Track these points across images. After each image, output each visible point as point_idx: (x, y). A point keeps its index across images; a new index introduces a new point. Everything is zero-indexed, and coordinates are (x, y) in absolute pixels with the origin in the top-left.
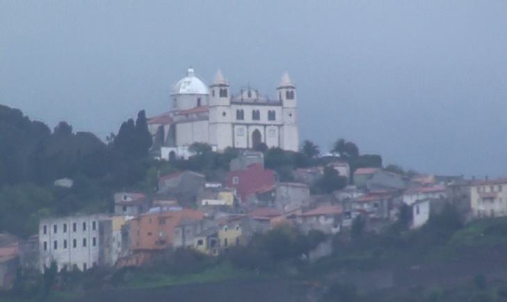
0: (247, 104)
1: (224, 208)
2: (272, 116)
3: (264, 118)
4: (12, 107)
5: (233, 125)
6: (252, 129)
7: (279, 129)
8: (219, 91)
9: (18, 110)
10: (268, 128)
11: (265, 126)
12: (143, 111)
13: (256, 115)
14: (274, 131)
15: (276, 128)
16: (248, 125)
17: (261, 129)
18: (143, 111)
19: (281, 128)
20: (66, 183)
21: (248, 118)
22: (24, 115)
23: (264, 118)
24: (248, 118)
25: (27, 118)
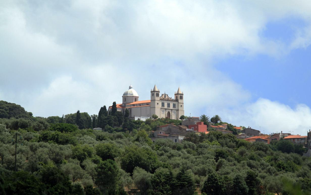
0: (165, 100)
1: (36, 137)
2: (174, 106)
3: (171, 107)
4: (17, 104)
5: (161, 108)
6: (168, 111)
7: (177, 111)
8: (167, 103)
9: (24, 108)
10: (173, 111)
11: (172, 110)
12: (115, 102)
13: (169, 105)
14: (175, 112)
15: (176, 111)
16: (166, 109)
17: (170, 111)
18: (115, 102)
19: (178, 111)
20: (212, 190)
21: (166, 106)
22: (47, 118)
23: (171, 107)
24: (166, 106)
25: (26, 111)
